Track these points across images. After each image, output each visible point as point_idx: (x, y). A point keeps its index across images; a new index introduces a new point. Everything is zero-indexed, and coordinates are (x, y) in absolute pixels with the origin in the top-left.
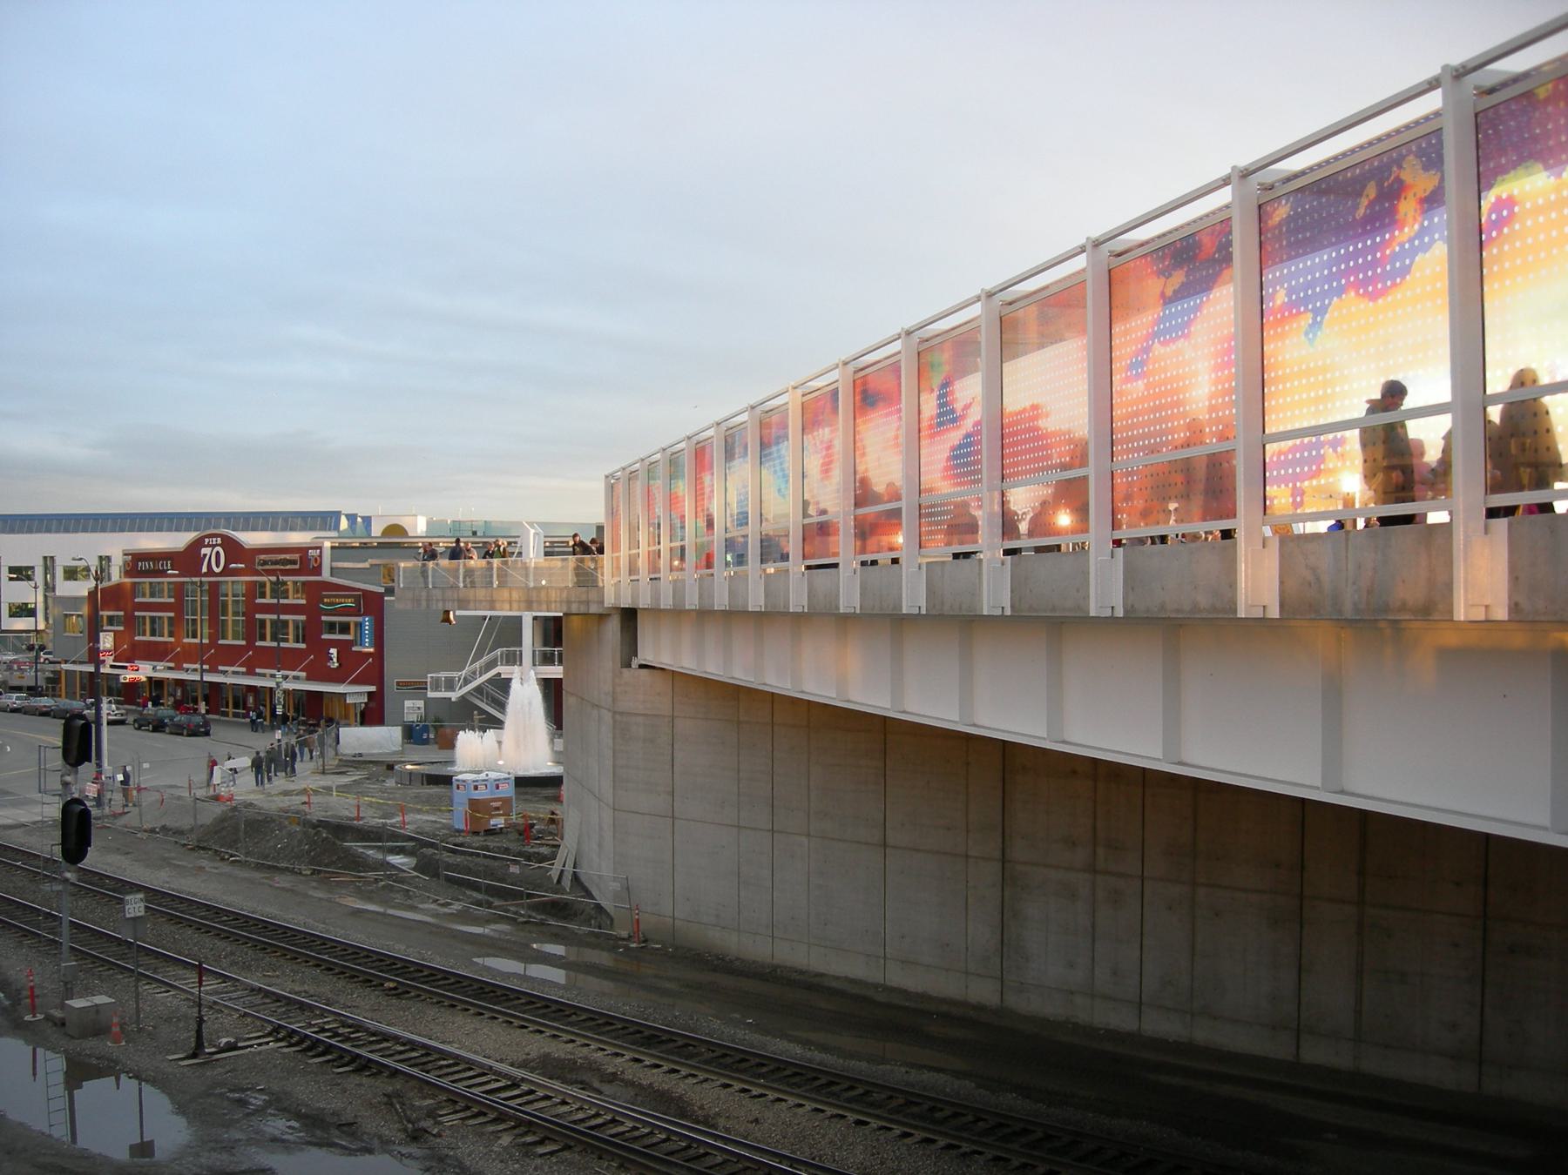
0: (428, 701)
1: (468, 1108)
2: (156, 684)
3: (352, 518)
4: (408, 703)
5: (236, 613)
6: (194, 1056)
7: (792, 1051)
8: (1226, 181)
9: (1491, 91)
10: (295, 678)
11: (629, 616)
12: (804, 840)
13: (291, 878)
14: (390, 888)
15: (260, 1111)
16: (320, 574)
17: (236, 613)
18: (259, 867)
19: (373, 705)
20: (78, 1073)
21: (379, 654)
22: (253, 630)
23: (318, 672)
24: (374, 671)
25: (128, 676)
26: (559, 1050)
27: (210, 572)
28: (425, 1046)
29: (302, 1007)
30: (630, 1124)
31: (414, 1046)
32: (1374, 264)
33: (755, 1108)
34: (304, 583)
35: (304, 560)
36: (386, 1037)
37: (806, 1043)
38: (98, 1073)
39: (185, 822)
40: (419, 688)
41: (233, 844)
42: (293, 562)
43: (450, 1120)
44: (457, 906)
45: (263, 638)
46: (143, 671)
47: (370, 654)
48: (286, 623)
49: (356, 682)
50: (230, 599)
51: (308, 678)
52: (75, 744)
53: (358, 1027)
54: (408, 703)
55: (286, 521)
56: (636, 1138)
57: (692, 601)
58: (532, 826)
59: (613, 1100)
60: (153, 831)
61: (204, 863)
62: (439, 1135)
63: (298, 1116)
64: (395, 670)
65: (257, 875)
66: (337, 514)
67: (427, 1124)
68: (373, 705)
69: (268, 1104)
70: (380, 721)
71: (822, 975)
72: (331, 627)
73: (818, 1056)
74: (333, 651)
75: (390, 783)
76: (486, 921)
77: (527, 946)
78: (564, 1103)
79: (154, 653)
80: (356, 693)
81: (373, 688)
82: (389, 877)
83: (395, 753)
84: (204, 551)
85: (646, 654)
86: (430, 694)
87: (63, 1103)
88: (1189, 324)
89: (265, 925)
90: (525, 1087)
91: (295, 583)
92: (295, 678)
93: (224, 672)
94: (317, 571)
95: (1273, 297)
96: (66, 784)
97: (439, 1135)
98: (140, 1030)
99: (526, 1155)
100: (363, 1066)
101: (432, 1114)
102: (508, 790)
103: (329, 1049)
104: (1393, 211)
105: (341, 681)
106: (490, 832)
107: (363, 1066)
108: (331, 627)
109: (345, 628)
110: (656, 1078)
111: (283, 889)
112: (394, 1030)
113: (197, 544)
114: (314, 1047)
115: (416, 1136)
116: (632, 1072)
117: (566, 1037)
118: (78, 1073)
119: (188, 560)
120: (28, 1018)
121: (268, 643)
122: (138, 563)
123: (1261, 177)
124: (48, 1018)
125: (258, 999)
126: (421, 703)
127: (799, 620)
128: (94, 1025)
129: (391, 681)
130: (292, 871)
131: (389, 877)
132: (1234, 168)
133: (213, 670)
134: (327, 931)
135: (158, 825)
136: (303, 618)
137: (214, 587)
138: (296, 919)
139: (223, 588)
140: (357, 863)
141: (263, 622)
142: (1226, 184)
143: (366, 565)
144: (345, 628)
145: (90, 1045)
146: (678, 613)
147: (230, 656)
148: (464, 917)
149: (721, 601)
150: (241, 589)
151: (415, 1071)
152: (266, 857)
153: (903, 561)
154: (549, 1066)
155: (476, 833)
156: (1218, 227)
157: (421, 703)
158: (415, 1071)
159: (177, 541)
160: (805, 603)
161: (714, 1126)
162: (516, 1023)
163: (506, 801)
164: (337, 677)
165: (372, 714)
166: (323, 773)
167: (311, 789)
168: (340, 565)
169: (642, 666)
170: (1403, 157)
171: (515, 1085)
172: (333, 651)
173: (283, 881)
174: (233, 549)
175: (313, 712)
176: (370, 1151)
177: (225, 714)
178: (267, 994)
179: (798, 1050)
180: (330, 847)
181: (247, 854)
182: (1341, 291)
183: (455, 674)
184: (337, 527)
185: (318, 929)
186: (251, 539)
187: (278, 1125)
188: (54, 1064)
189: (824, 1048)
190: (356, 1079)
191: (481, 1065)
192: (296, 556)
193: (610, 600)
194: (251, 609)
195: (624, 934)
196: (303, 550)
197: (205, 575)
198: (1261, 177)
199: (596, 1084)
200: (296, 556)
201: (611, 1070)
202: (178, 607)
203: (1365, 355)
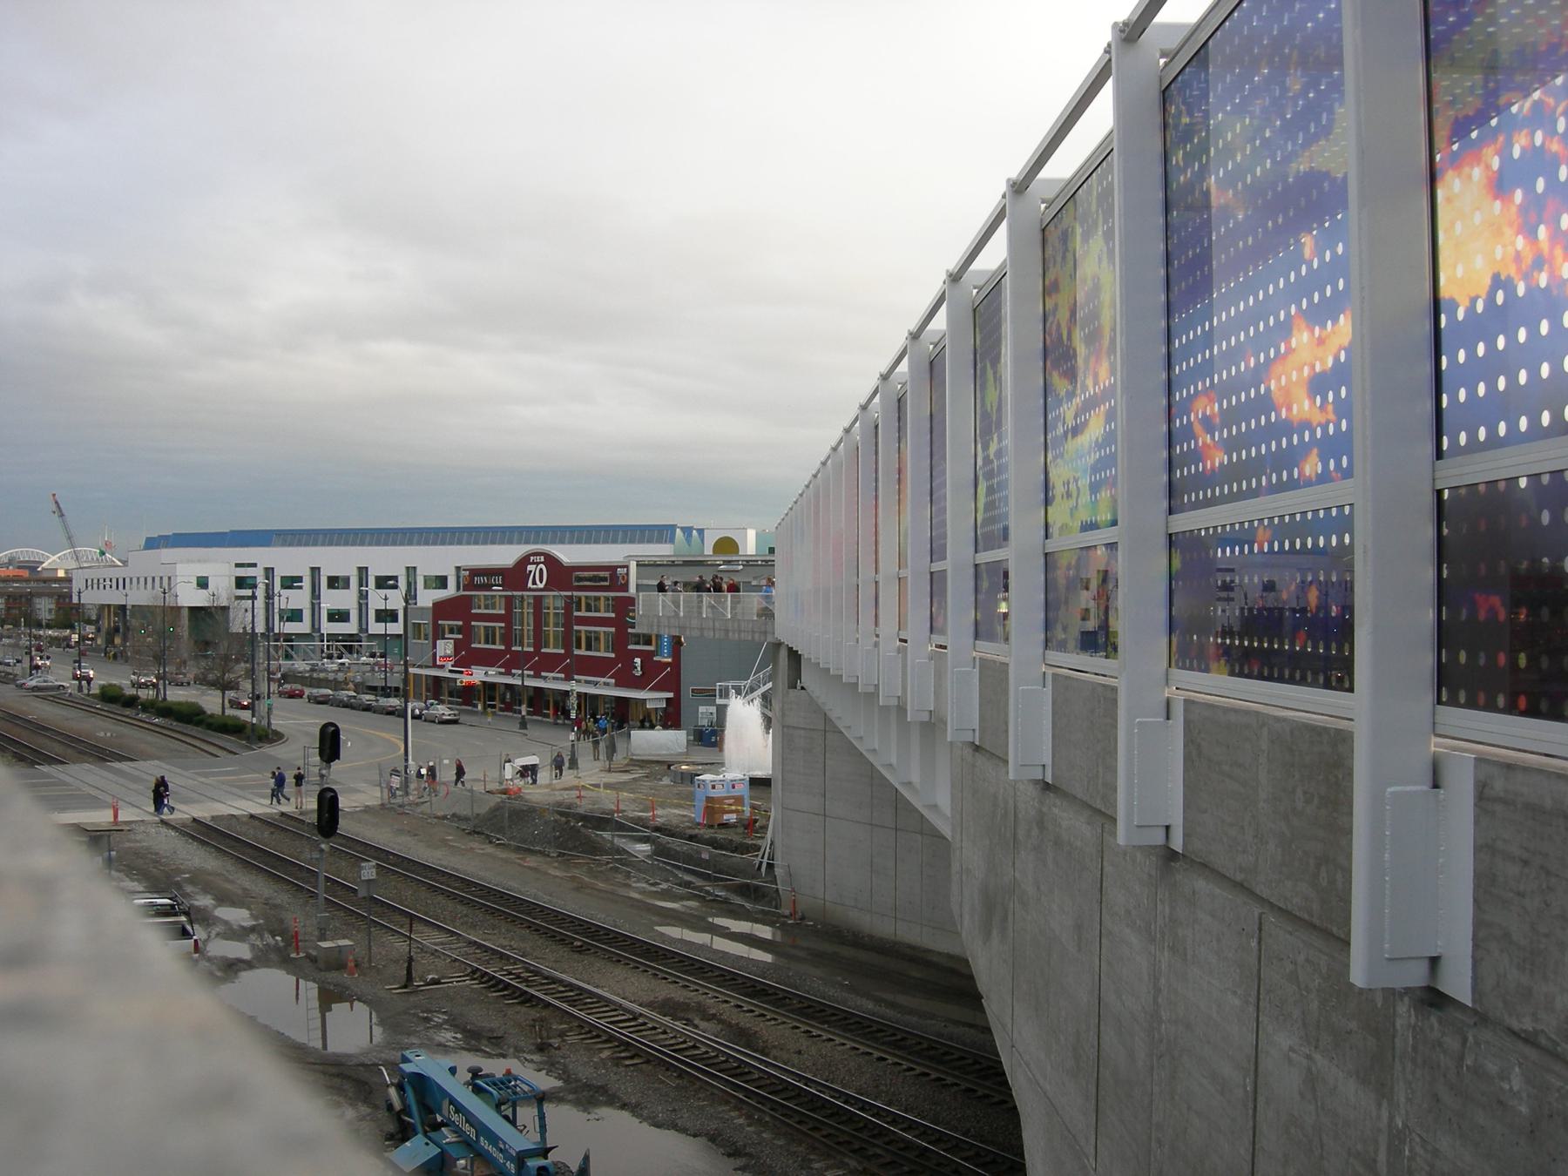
1: (598, 1036)
2: (489, 687)
3: (687, 531)
4: (702, 709)
5: (556, 625)
6: (405, 987)
7: (862, 1005)
10: (606, 684)
12: (919, 837)
13: (540, 859)
14: (616, 870)
15: (439, 1027)
16: (627, 590)
17: (556, 625)
18: (518, 849)
19: (671, 710)
20: (328, 998)
21: (676, 665)
22: (569, 640)
23: (624, 680)
24: (672, 681)
25: (464, 679)
26: (679, 995)
28: (580, 988)
29: (502, 956)
30: (704, 1049)
31: (571, 987)
33: (804, 1043)
34: (614, 599)
36: (555, 981)
37: (878, 1001)
38: (341, 998)
39: (464, 810)
41: (501, 830)
42: (605, 579)
43: (572, 1038)
44: (664, 886)
45: (579, 647)
46: (478, 675)
47: (668, 664)
49: (655, 689)
50: (552, 611)
51: (617, 685)
52: (328, 745)
53: (537, 973)
54: (702, 709)
55: (625, 533)
56: (742, 1074)
58: (756, 821)
59: (705, 1033)
60: (444, 817)
61: (475, 845)
62: (559, 1048)
63: (464, 1031)
64: (690, 680)
65: (513, 856)
66: (674, 527)
67: (555, 1042)
68: (671, 710)
69: (446, 1022)
70: (676, 725)
71: (930, 951)
73: (883, 1010)
74: (638, 660)
75: (666, 781)
76: (682, 898)
77: (704, 919)
78: (665, 1032)
79: (487, 659)
80: (654, 699)
81: (671, 695)
82: (620, 861)
83: (680, 754)
84: (530, 568)
87: (318, 1023)
89: (502, 896)
90: (641, 1020)
91: (607, 599)
92: (606, 684)
93: (545, 678)
95: (1055, 428)
96: (322, 776)
97: (559, 1048)
98: (371, 968)
99: (617, 1065)
100: (527, 999)
101: (562, 1034)
102: (743, 790)
103: (507, 986)
105: (642, 688)
106: (725, 825)
107: (527, 999)
110: (745, 1020)
111: (530, 868)
112: (563, 976)
113: (525, 561)
114: (495, 984)
115: (542, 1048)
116: (727, 1011)
117: (693, 987)
118: (328, 998)
119: (515, 576)
120: (293, 955)
121: (582, 652)
122: (476, 578)
124: (308, 956)
125: (471, 950)
126: (713, 709)
128: (337, 962)
129: (687, 690)
130: (542, 853)
131: (620, 861)
134: (550, 902)
135: (449, 813)
137: (538, 601)
138: (530, 891)
139: (546, 602)
140: (594, 848)
145: (333, 976)
147: (550, 663)
148: (667, 895)
150: (560, 603)
151: (564, 1006)
152: (524, 842)
154: (670, 1008)
155: (711, 827)
158: (564, 1006)
159: (505, 556)
161: (767, 1055)
162: (661, 975)
163: (739, 800)
164: (639, 684)
165: (671, 718)
166: (609, 771)
167: (591, 780)
168: (645, 582)
171: (635, 1019)
172: (638, 660)
173: (532, 861)
175: (623, 715)
176: (504, 1056)
177: (547, 716)
178: (479, 946)
179: (870, 1005)
180: (577, 834)
181: (510, 839)
183: (743, 683)
184: (672, 540)
185: (544, 901)
186: (568, 554)
187: (447, 1036)
188: (310, 990)
189: (892, 1005)
190: (523, 1009)
191: (614, 1003)
192: (606, 574)
194: (568, 620)
195: (787, 912)
199: (696, 1022)
200: (606, 574)
201: (713, 1011)
202: (507, 618)
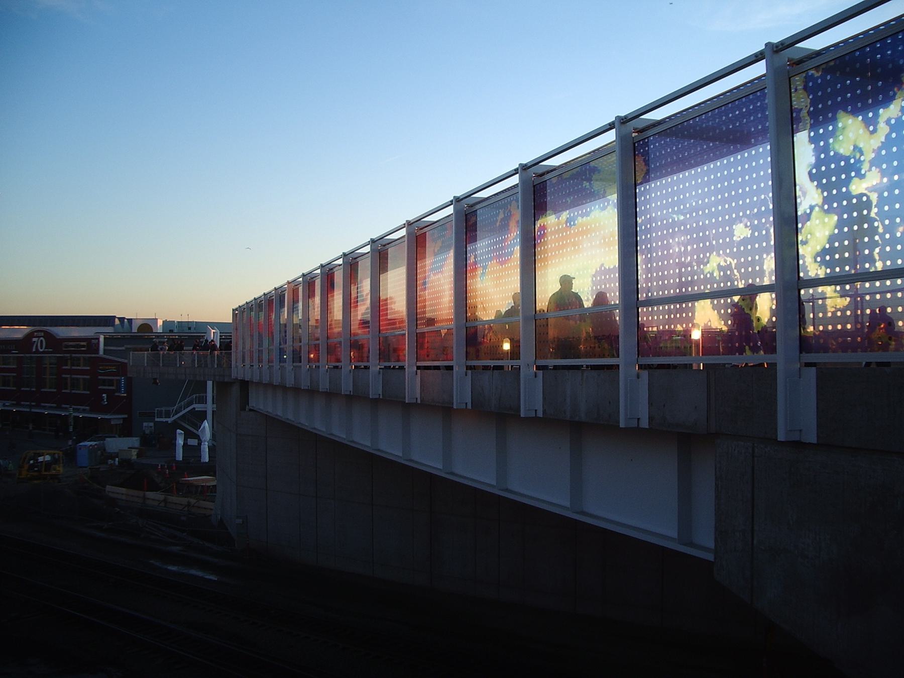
0: (156, 423)
4: (145, 424)
8: (611, 126)
9: (542, 175)
11: (245, 385)
27: (37, 352)
32: (502, 248)
35: (91, 344)
40: (150, 416)
42: (83, 346)
48: (78, 379)
54: (145, 424)
57: (324, 385)
72: (104, 382)
80: (116, 419)
81: (126, 416)
84: (34, 339)
85: (252, 404)
86: (157, 419)
88: (442, 266)
94: (97, 350)
104: (508, 225)
108: (104, 382)
109: (111, 383)
113: (30, 336)
119: (25, 343)
123: (788, 53)
126: (152, 424)
127: (408, 408)
132: (520, 164)
133: (38, 406)
136: (88, 377)
141: (66, 379)
142: (611, 129)
143: (123, 348)
144: (111, 383)
146: (270, 385)
149: (305, 384)
153: (456, 369)
156: (847, 58)
157: (152, 424)
160: (418, 396)
165: (126, 430)
169: (251, 410)
170: (511, 201)
174: (49, 336)
182: (491, 259)
193: (233, 376)
196: (88, 340)
197: (34, 353)
198: (538, 169)
203: (711, 246)
